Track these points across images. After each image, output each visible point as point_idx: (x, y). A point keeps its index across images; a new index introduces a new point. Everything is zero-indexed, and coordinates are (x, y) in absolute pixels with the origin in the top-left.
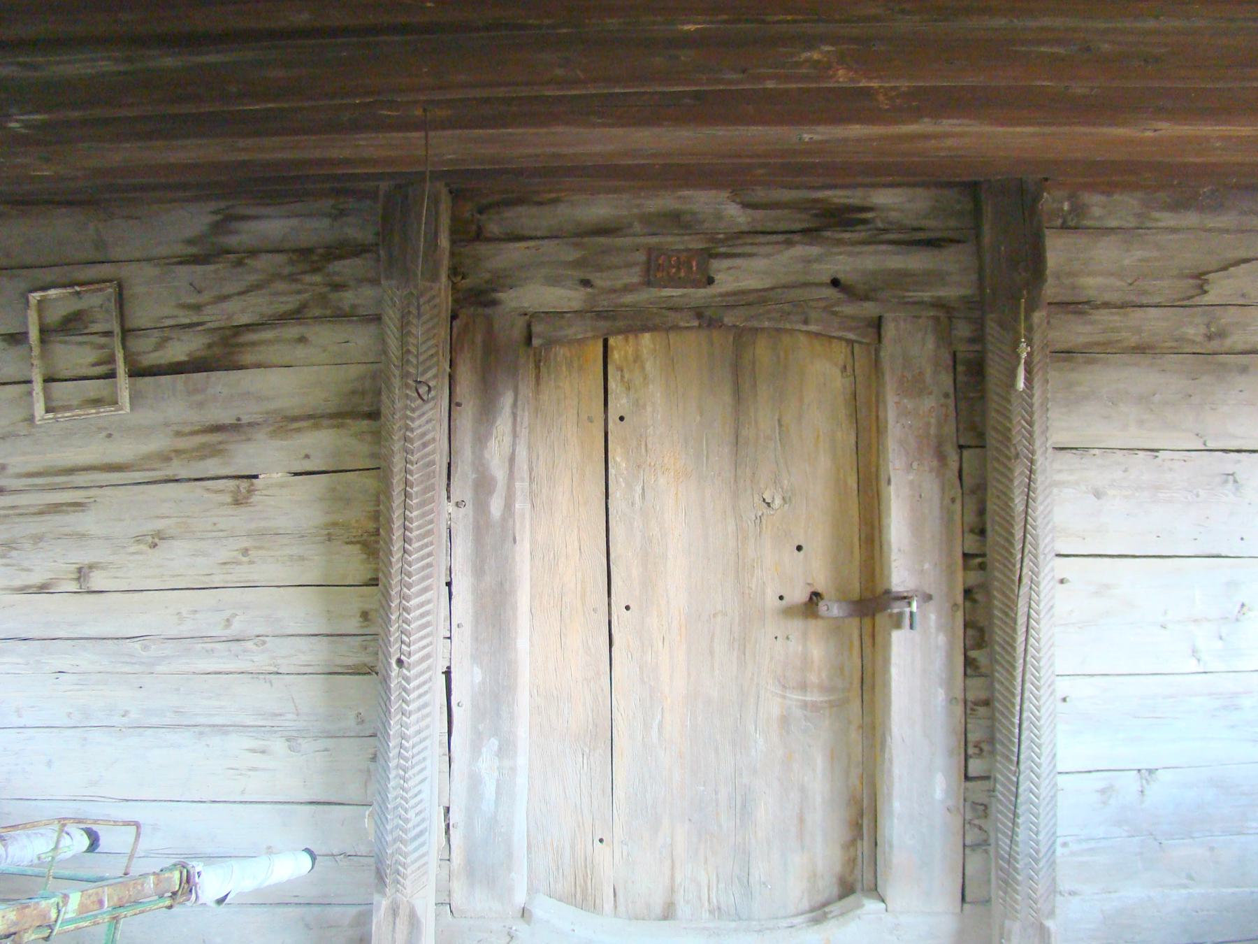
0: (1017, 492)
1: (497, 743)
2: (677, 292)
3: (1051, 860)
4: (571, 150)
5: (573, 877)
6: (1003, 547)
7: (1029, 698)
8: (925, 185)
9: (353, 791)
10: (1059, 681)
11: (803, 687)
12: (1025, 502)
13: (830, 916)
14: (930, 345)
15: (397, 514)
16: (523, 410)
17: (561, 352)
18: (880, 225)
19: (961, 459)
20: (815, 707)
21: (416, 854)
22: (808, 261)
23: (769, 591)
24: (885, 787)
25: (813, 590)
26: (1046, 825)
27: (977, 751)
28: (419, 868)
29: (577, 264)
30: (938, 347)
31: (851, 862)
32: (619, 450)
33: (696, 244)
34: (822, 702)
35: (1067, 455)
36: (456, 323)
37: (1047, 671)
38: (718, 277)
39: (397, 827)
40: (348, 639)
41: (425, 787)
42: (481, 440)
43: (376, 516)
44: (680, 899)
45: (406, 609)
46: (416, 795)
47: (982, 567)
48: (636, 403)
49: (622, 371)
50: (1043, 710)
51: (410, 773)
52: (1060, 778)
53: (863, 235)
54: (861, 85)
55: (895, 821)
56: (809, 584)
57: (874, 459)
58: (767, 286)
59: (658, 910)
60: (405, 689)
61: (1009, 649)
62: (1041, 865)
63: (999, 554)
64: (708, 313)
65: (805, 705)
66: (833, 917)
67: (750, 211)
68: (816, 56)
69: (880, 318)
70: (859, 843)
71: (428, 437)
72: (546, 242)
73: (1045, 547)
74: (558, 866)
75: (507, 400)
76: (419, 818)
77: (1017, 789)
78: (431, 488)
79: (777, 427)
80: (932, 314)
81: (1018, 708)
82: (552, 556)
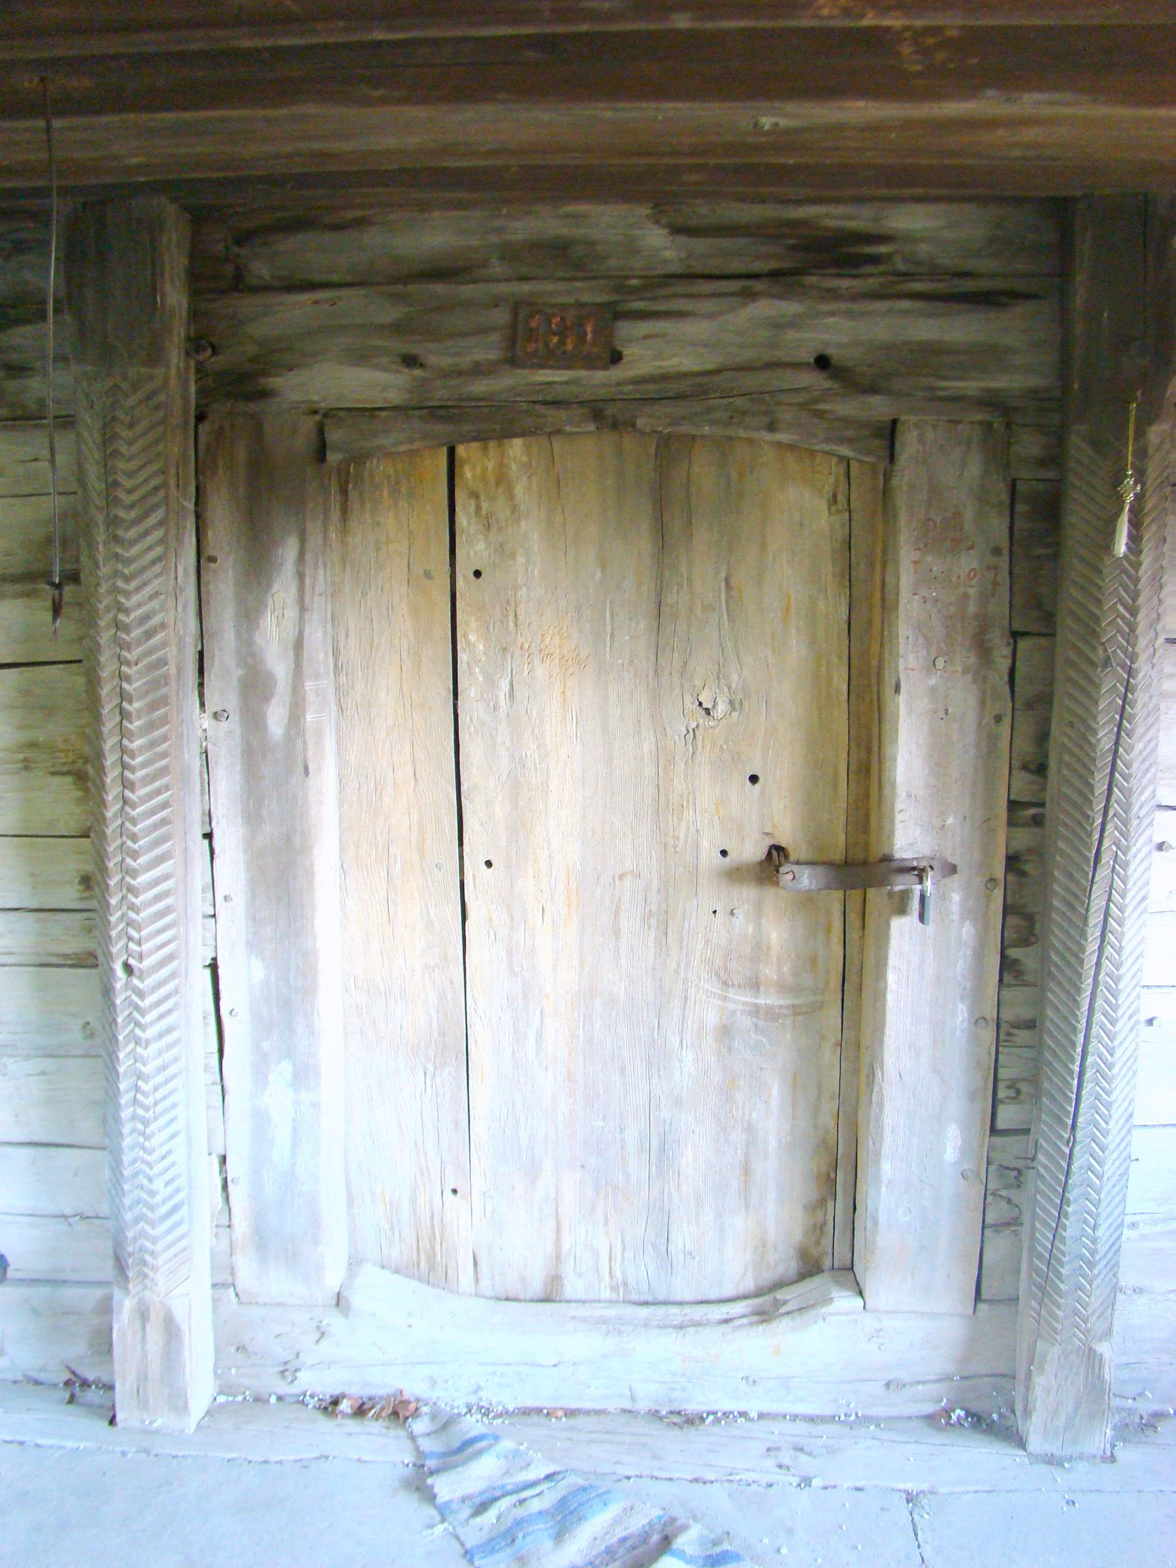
3: (1112, 1263)
4: (346, 147)
5: (414, 1240)
6: (1075, 805)
7: (1098, 1035)
8: (983, 200)
9: (86, 1130)
11: (755, 985)
12: (1114, 737)
13: (783, 1310)
14: (975, 467)
16: (316, 566)
18: (901, 266)
20: (771, 1014)
21: (170, 1238)
22: (777, 325)
23: (705, 843)
24: (870, 1142)
25: (772, 842)
26: (1108, 1217)
27: (1011, 1093)
28: (176, 1255)
29: (399, 328)
30: (986, 473)
31: (818, 1229)
32: (473, 625)
33: (591, 294)
34: (781, 1007)
36: (205, 428)
38: (626, 352)
39: (139, 1201)
40: (64, 916)
42: (249, 615)
45: (131, 890)
46: (164, 1158)
47: (1037, 821)
48: (501, 549)
49: (477, 497)
50: (1118, 1053)
51: (153, 1127)
53: (872, 283)
54: (865, 23)
55: (884, 1189)
56: (767, 834)
57: (875, 647)
58: (709, 367)
60: (137, 1008)
61: (1073, 960)
62: (1096, 1271)
63: (1067, 813)
64: (611, 410)
65: (755, 1011)
66: (787, 1313)
67: (682, 240)
69: (894, 423)
70: (830, 1204)
71: (155, 621)
72: (345, 292)
73: (1141, 807)
74: (392, 1224)
75: (289, 552)
76: (170, 1188)
77: (1069, 1165)
79: (723, 588)
80: (979, 417)
81: (1079, 1049)
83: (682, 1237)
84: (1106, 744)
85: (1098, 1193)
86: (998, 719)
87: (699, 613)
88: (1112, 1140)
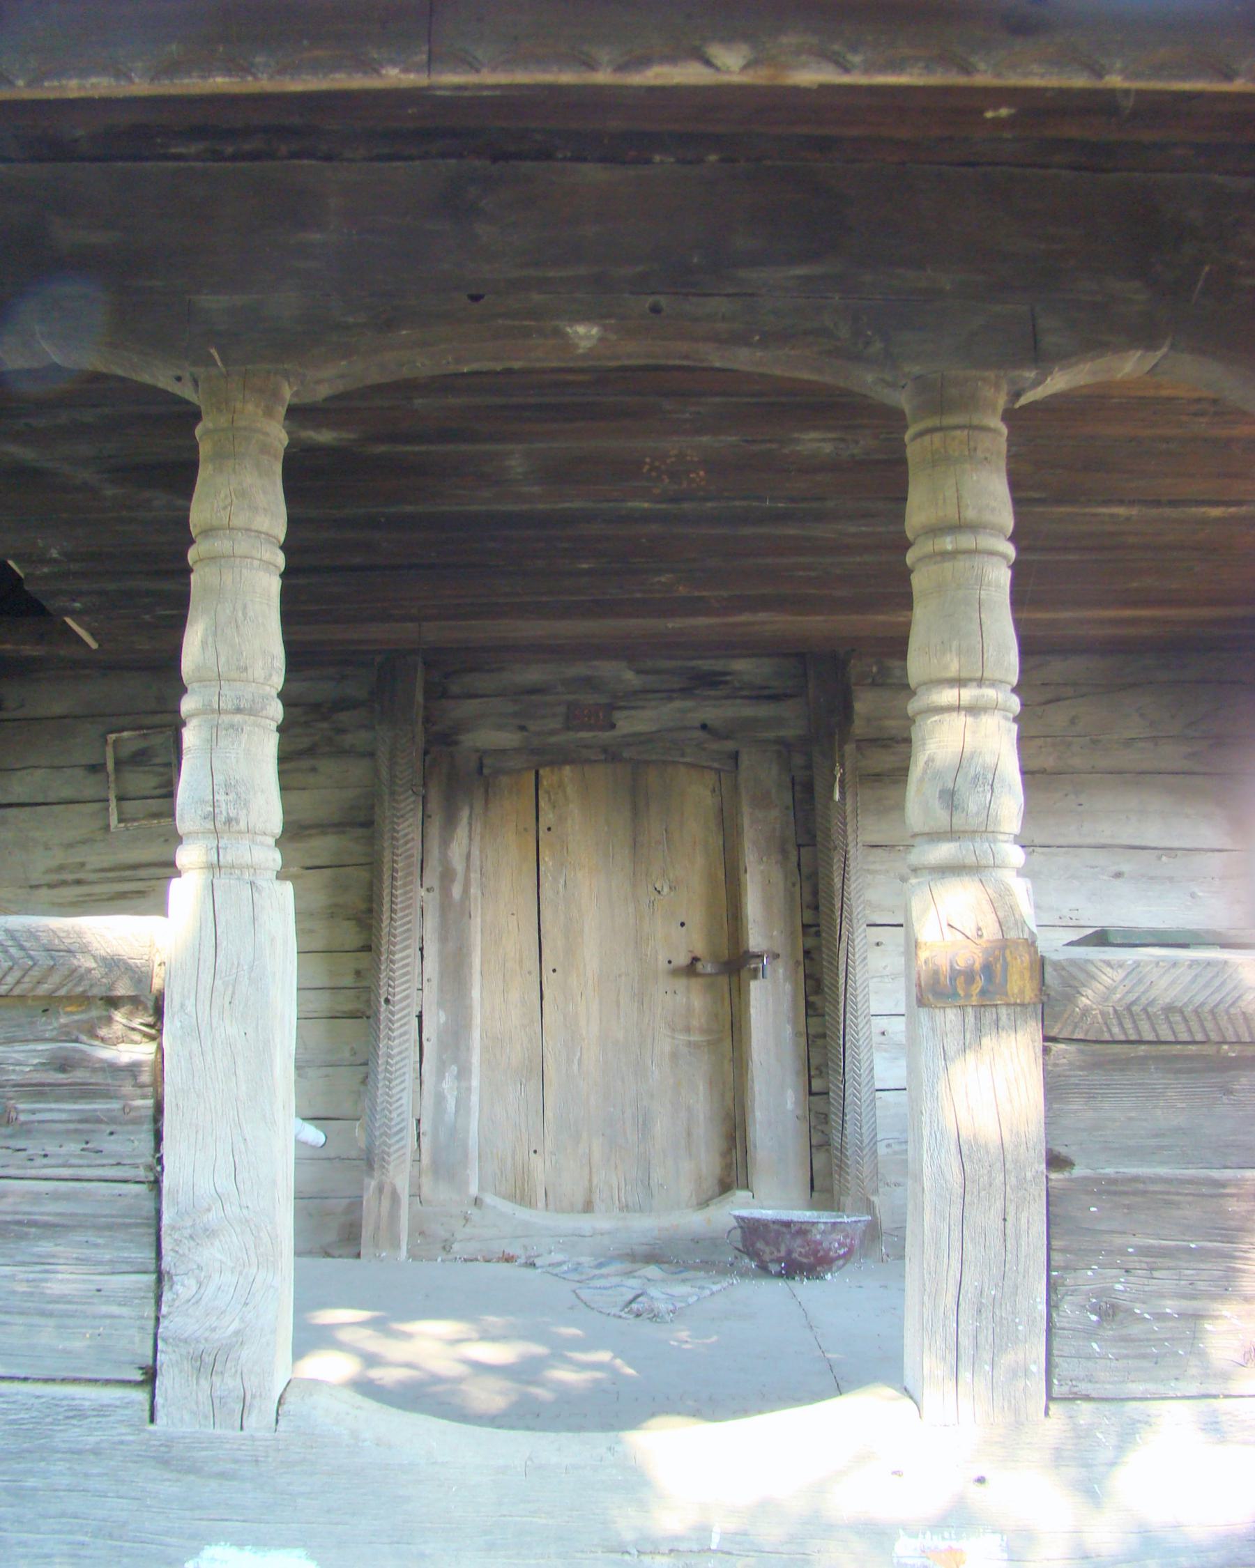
0: (836, 874)
1: (456, 1068)
2: (591, 734)
10: (875, 1020)
11: (688, 1030)
15: (386, 892)
17: (505, 780)
18: (737, 685)
19: (799, 854)
23: (660, 957)
25: (694, 955)
26: (868, 1122)
27: (818, 1072)
31: (728, 1167)
32: (547, 853)
33: (603, 700)
35: (879, 851)
36: (428, 758)
37: (863, 1005)
38: (619, 724)
41: (404, 1094)
42: (445, 843)
43: (370, 899)
44: (596, 1198)
45: (392, 961)
47: (818, 934)
50: (861, 1035)
51: (394, 1083)
52: (878, 1094)
55: (758, 1126)
59: (580, 1206)
60: (391, 1021)
62: (865, 1152)
65: (689, 1044)
68: (663, 579)
70: (734, 1151)
71: (410, 837)
73: (858, 914)
75: (465, 814)
76: (399, 1119)
78: (410, 874)
81: (842, 1032)
82: (497, 932)
83: (657, 1175)
84: (839, 885)
85: (860, 1109)
86: (794, 885)
87: (653, 845)
88: (864, 1081)
